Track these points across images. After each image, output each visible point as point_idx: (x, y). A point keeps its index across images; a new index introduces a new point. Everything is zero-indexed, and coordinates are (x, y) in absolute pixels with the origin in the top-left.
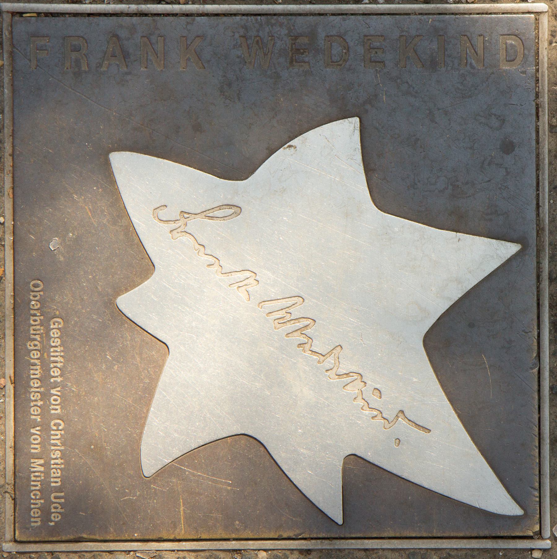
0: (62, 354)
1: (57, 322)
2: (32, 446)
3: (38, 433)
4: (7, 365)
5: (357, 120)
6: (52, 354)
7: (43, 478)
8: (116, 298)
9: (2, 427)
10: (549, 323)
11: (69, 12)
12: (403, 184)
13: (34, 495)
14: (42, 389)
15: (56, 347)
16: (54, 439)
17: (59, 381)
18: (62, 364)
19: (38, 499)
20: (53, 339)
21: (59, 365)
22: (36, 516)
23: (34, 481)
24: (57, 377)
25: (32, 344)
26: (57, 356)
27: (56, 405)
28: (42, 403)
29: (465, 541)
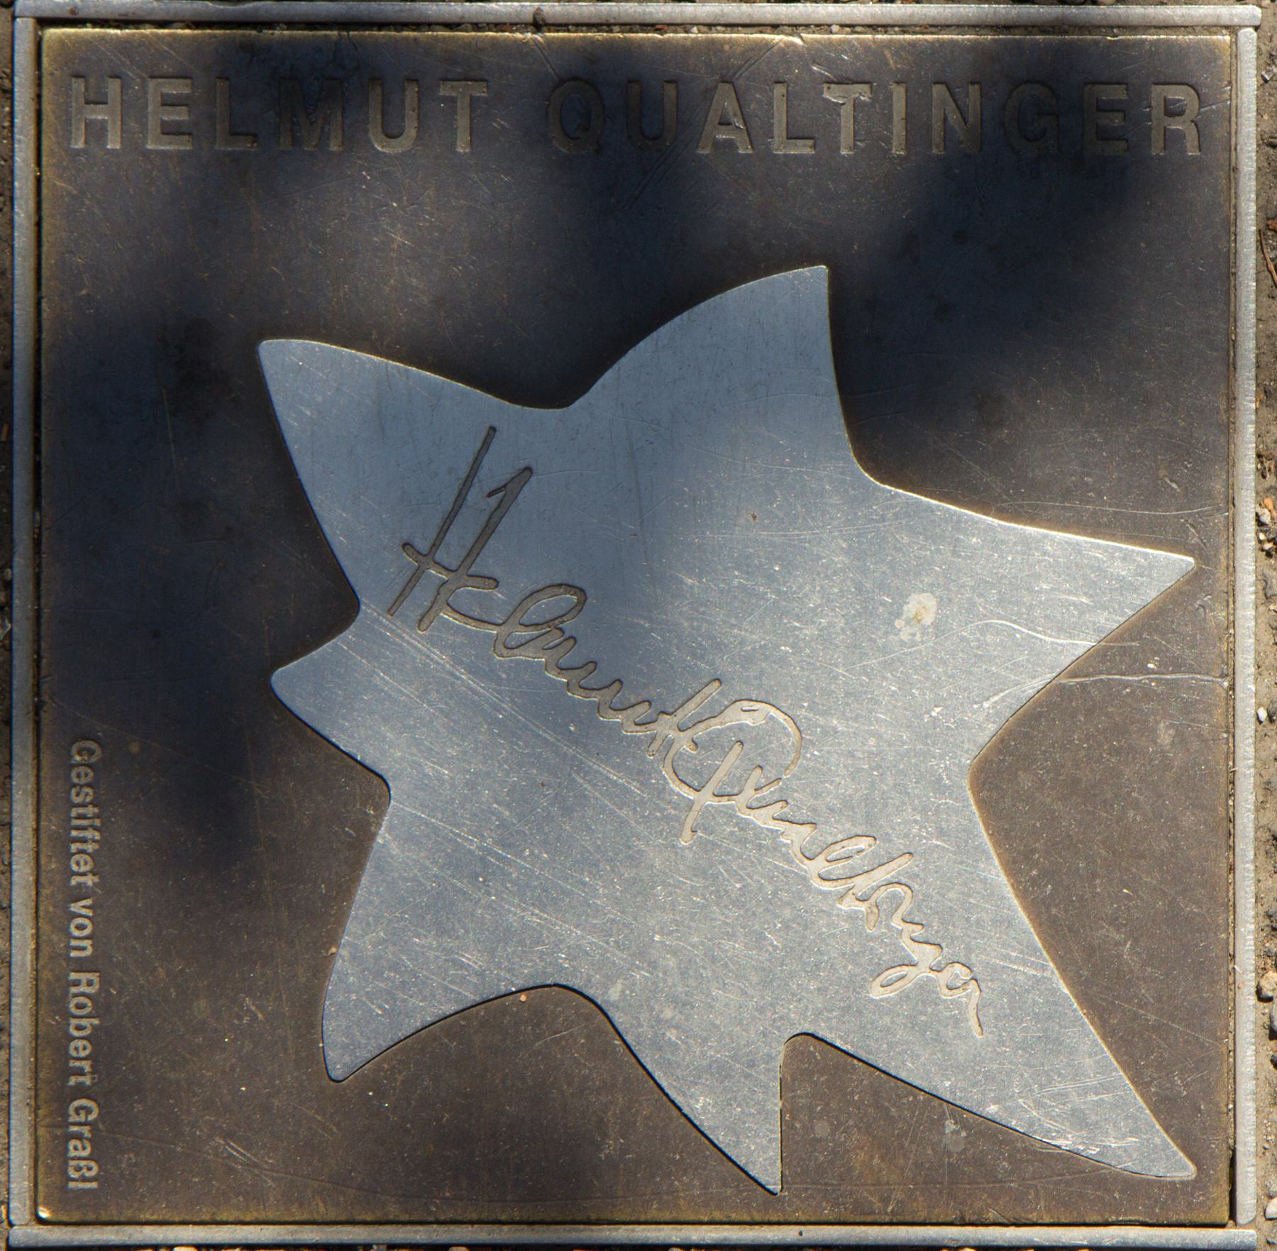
0: (97, 822)
8: (263, 337)
9: (7, 83)
11: (587, 21)
18: (96, 846)
24: (83, 874)
26: (84, 828)
27: (82, 1017)
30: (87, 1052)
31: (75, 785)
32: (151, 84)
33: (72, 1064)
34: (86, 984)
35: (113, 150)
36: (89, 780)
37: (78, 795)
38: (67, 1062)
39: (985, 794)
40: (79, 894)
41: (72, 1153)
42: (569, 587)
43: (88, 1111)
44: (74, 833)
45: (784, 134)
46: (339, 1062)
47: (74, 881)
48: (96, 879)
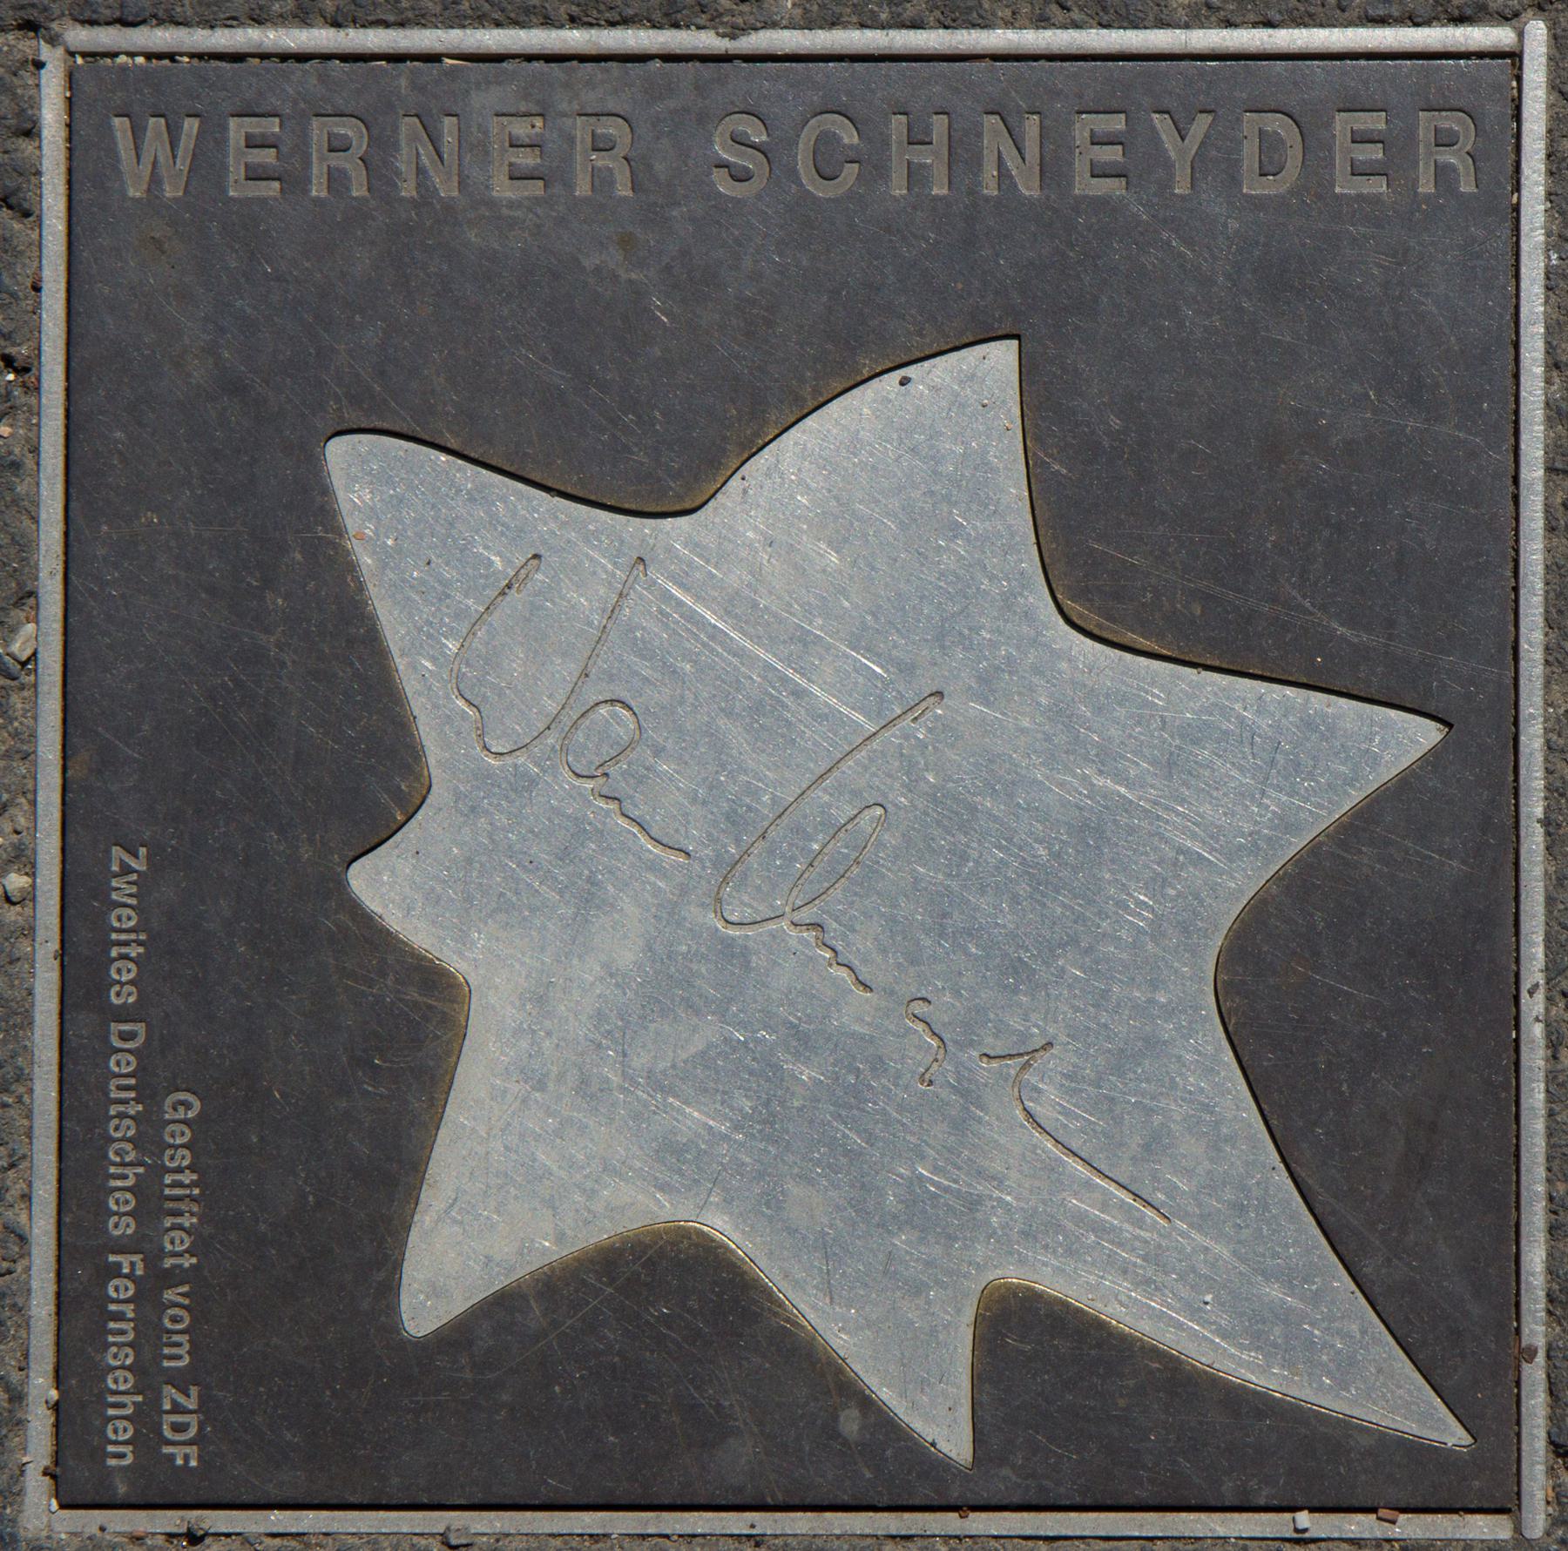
0: (196, 1191)
1: (182, 1103)
3: (187, 1302)
6: (167, 1192)
12: (1152, 544)
13: (117, 1153)
15: (179, 1170)
17: (187, 1265)
19: (131, 1164)
20: (169, 1152)
22: (124, 1071)
24: (179, 1255)
28: (140, 1108)
29: (1138, 647)
30: (131, 1293)
32: (315, 123)
33: (113, 1307)
35: (318, 198)
36: (185, 1140)
37: (116, 1129)
40: (170, 1278)
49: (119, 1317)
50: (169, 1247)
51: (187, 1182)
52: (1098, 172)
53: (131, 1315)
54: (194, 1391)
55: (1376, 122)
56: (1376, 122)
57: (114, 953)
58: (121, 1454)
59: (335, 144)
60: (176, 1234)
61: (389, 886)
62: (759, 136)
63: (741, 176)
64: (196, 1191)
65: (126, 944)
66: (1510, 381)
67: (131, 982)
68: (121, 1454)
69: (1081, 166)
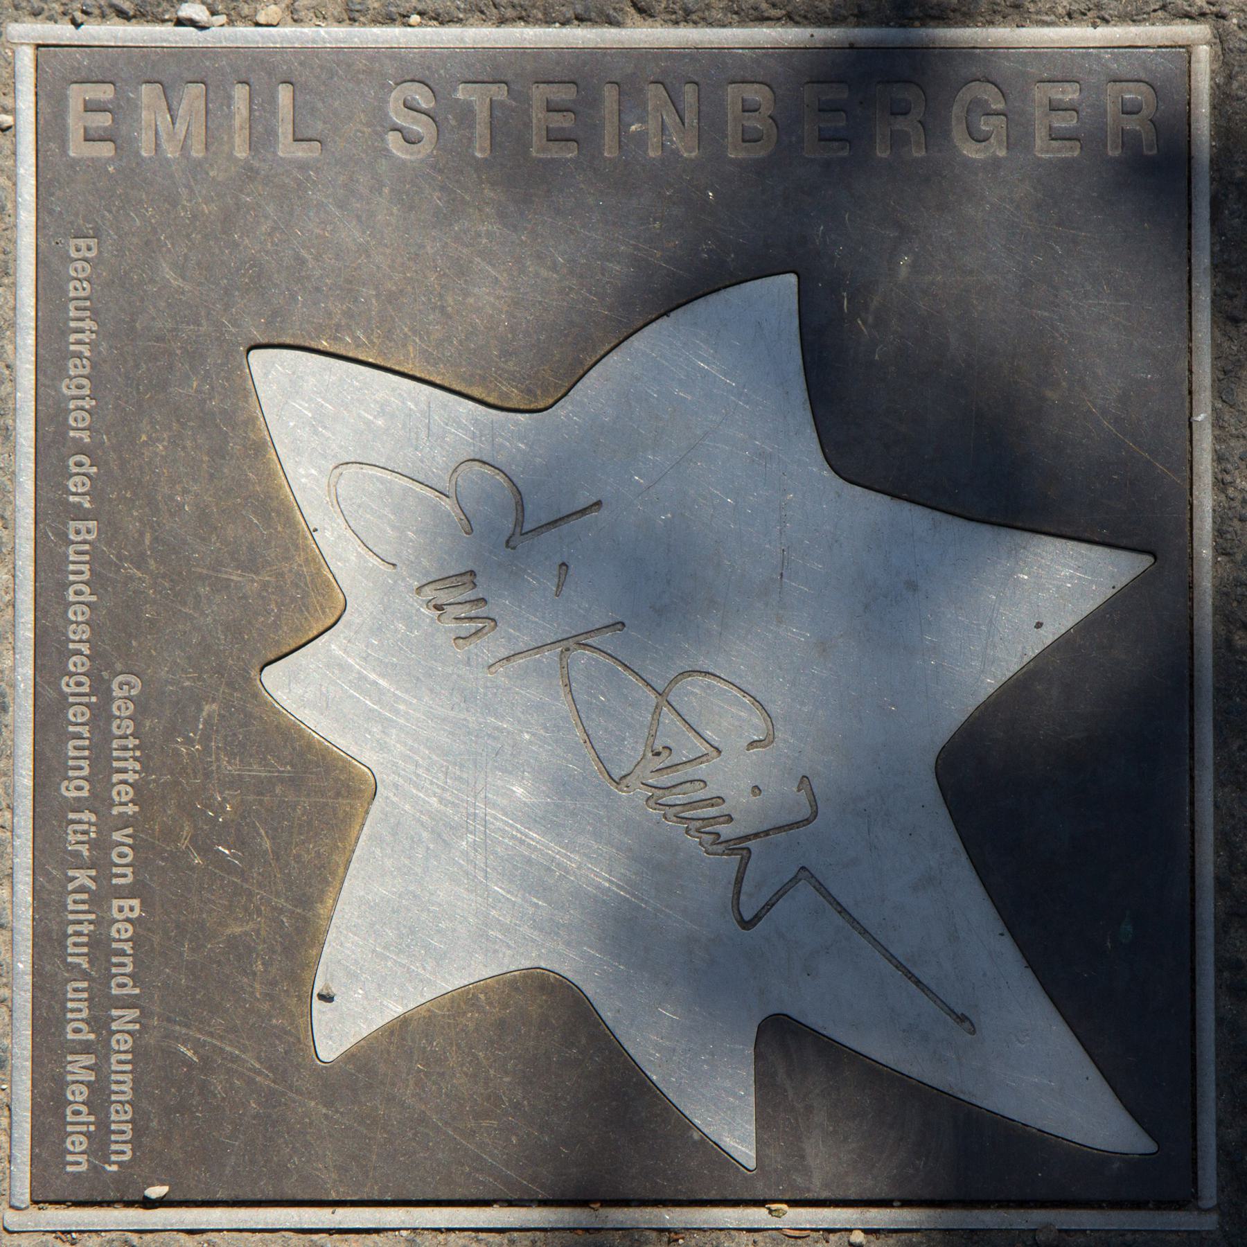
0: (138, 753)
1: (128, 684)
2: (69, 1158)
3: (130, 841)
4: (21, 226)
5: (792, 279)
7: (93, 835)
10: (1215, 834)
14: (94, 699)
16: (117, 1142)
21: (84, 337)
23: (73, 912)
25: (72, 683)
26: (126, 760)
31: (73, 622)
34: (84, 532)
38: (97, 1118)
39: (1217, 432)
41: (72, 294)
42: (757, 918)
43: (126, 856)
44: (71, 917)
45: (290, 137)
46: (271, 372)
47: (115, 811)
48: (136, 809)
49: (123, 953)
50: (117, 799)
51: (131, 746)
52: (553, 137)
53: (87, 652)
54: (71, 873)
55: (105, 93)
56: (105, 93)
57: (70, 931)
58: (78, 1163)
59: (90, 107)
60: (122, 787)
61: (302, 689)
62: (690, 151)
63: (411, 140)
64: (138, 753)
65: (80, 922)
66: (40, 93)
67: (129, 718)
68: (78, 1163)
69: (537, 138)
